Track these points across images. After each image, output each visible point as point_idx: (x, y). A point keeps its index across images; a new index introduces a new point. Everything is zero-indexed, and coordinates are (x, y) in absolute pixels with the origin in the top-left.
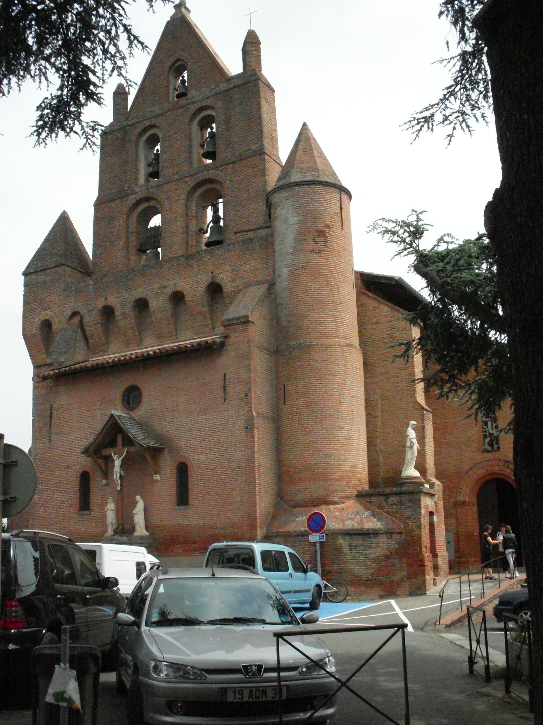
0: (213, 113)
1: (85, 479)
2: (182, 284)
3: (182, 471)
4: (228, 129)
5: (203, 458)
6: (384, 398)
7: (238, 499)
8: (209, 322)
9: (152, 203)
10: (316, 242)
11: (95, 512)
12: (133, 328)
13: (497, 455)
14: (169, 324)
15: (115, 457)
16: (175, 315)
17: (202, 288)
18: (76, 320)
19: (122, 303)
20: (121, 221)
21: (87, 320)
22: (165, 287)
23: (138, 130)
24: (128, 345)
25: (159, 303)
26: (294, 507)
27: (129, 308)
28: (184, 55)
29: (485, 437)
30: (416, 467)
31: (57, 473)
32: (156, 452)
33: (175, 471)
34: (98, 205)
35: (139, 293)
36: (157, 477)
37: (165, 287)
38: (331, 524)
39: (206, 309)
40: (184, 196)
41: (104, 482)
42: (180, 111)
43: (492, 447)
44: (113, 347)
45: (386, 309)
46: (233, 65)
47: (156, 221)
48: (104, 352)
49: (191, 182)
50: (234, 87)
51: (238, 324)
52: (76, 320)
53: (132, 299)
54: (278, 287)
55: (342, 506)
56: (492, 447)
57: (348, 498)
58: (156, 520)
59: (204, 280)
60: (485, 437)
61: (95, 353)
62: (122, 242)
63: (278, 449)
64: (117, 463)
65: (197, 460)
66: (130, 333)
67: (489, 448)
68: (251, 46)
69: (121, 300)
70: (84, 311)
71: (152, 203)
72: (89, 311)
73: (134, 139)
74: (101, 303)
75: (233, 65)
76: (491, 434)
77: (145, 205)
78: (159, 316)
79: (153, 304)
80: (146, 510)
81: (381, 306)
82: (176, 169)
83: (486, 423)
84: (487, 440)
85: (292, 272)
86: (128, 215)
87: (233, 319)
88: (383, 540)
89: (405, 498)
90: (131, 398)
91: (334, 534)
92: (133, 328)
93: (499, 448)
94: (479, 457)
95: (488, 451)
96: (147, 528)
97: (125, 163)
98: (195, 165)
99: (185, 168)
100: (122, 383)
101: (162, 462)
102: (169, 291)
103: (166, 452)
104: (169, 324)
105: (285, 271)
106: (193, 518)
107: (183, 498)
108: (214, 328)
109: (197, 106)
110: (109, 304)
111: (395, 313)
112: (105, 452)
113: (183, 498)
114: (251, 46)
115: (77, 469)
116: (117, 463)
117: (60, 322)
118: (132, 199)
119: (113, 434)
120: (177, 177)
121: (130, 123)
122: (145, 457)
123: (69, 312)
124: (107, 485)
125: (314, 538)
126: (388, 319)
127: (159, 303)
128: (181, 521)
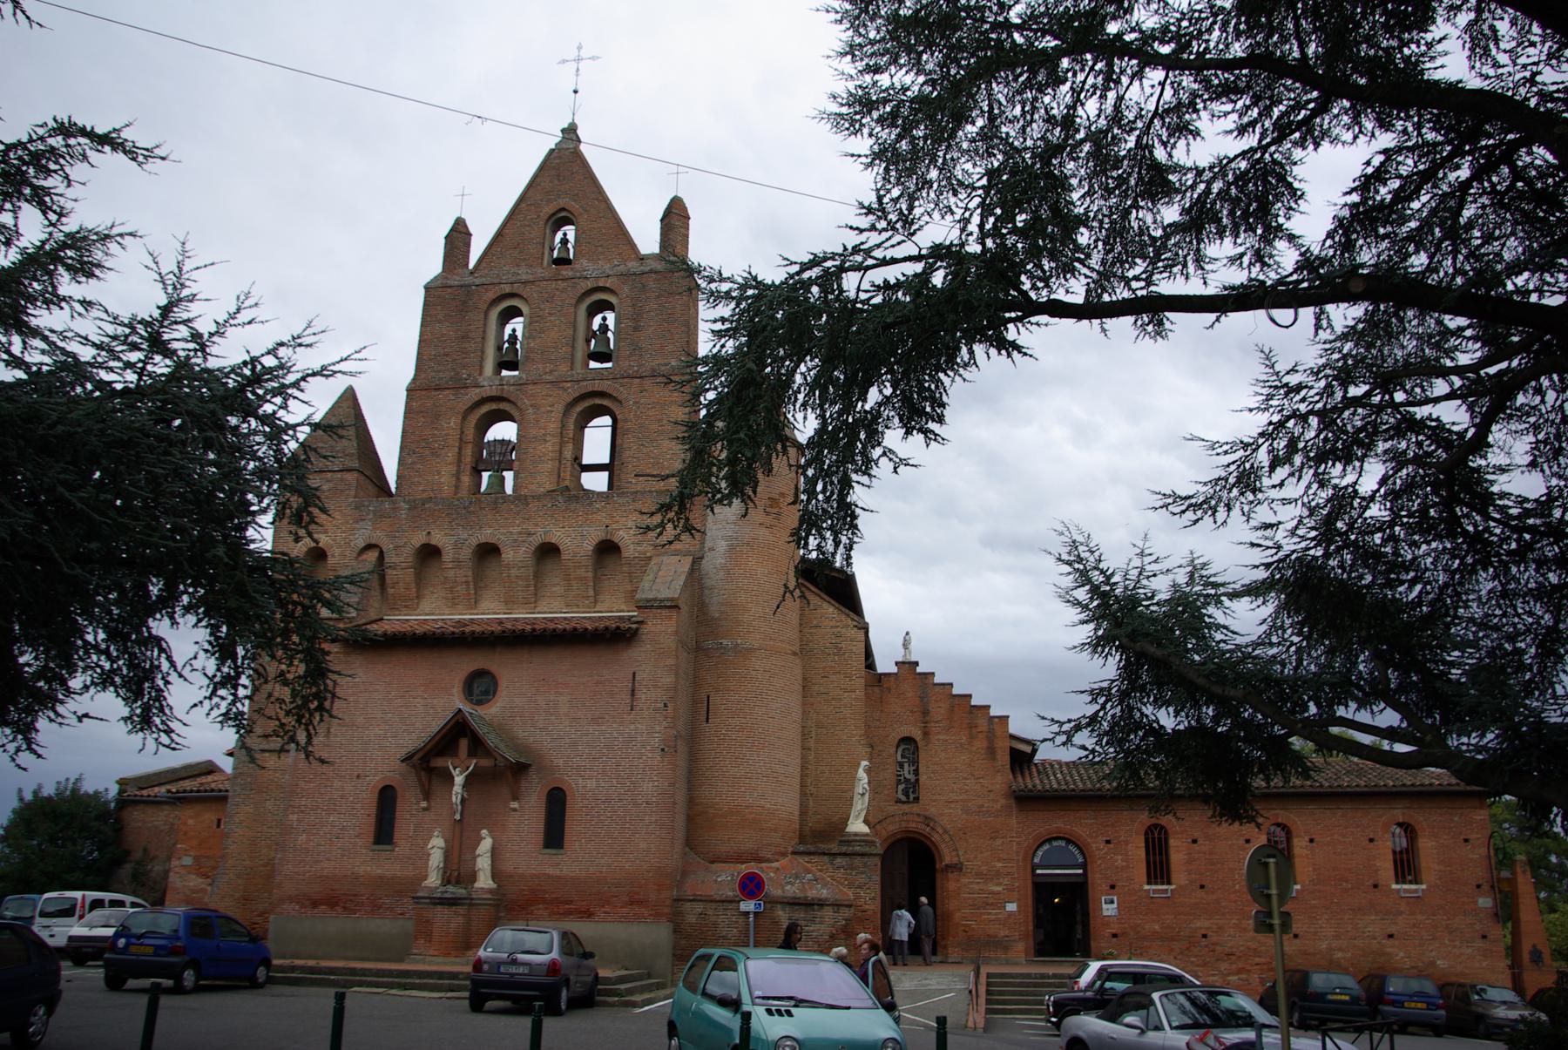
0: (613, 299)
1: (387, 799)
2: (558, 535)
3: (557, 802)
4: (636, 329)
5: (591, 784)
6: (819, 726)
7: (643, 845)
8: (591, 593)
9: (503, 406)
10: (768, 513)
11: (402, 846)
12: (467, 583)
13: (915, 808)
14: (528, 586)
15: (456, 772)
16: (538, 576)
17: (589, 546)
18: (372, 556)
19: (457, 545)
20: (454, 422)
21: (390, 558)
22: (529, 534)
23: (491, 295)
24: (453, 603)
25: (516, 555)
26: (712, 862)
27: (466, 553)
28: (574, 206)
29: (899, 782)
30: (866, 821)
31: (337, 784)
32: (520, 769)
33: (544, 799)
34: (414, 391)
35: (486, 535)
36: (515, 805)
37: (529, 534)
38: (772, 889)
39: (590, 574)
40: (560, 407)
41: (424, 804)
42: (561, 284)
43: (908, 796)
44: (426, 605)
45: (831, 609)
46: (648, 240)
47: (504, 431)
48: (411, 606)
49: (574, 391)
50: (651, 271)
51: (660, 607)
52: (372, 556)
53: (474, 542)
54: (706, 564)
55: (775, 865)
56: (908, 796)
57: (784, 855)
58: (508, 867)
59: (594, 535)
60: (899, 782)
61: (394, 609)
62: (451, 455)
63: (689, 782)
64: (459, 780)
65: (583, 787)
66: (461, 589)
67: (904, 798)
68: (675, 218)
69: (454, 541)
70: (387, 546)
71: (503, 406)
72: (396, 548)
73: (484, 307)
74: (419, 539)
75: (648, 240)
76: (907, 780)
77: (494, 406)
78: (514, 572)
79: (508, 555)
80: (495, 853)
81: (825, 605)
82: (549, 367)
83: (901, 765)
84: (901, 787)
85: (731, 548)
86: (464, 418)
87: (655, 600)
88: (828, 913)
89: (857, 861)
90: (480, 686)
91: (773, 902)
92: (467, 583)
93: (917, 799)
94: (893, 808)
95: (899, 801)
96: (494, 876)
97: (465, 338)
98: (579, 369)
99: (563, 368)
100: (468, 663)
101: (524, 784)
102: (537, 540)
103: (532, 770)
104: (528, 586)
105: (722, 545)
106: (572, 863)
107: (554, 836)
108: (596, 602)
109: (590, 284)
110: (433, 542)
111: (843, 617)
112: (438, 762)
113: (554, 836)
114: (675, 218)
115: (376, 780)
116: (459, 780)
117: (343, 555)
118: (474, 395)
119: (457, 734)
120: (549, 378)
121: (477, 282)
122: (503, 773)
123: (362, 544)
124: (425, 809)
125: (748, 906)
126: (833, 623)
127: (516, 555)
128: (550, 871)
